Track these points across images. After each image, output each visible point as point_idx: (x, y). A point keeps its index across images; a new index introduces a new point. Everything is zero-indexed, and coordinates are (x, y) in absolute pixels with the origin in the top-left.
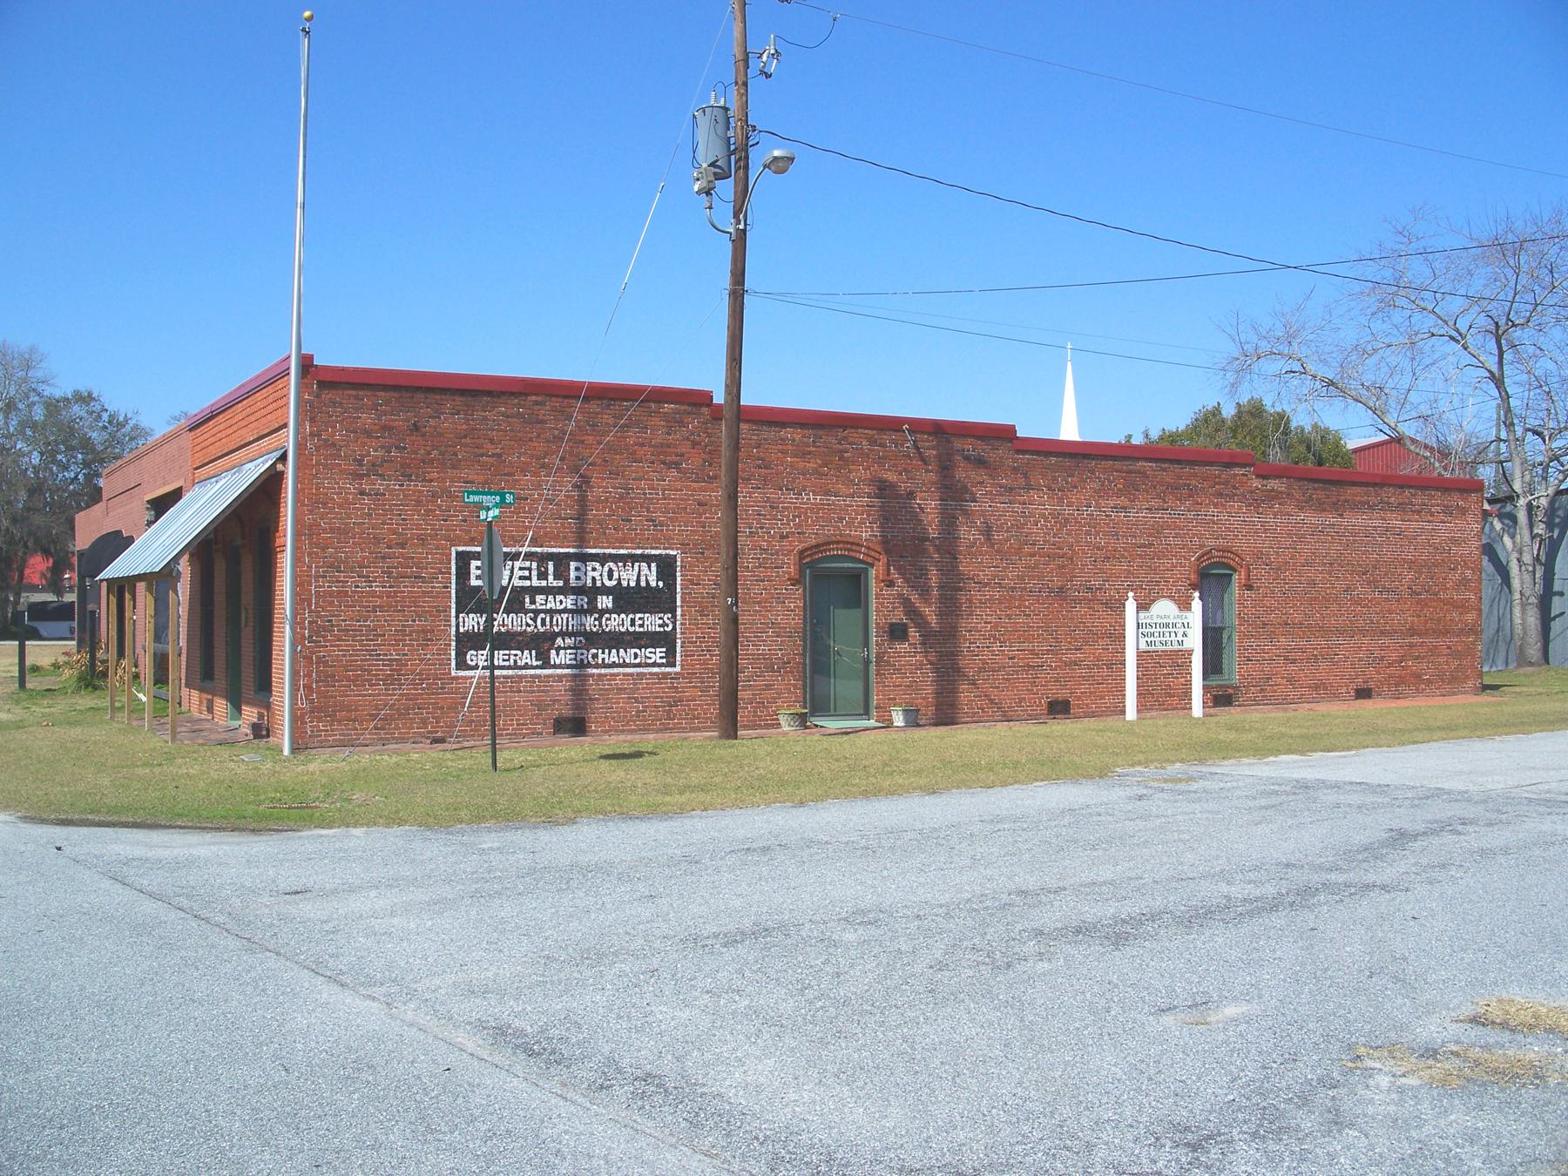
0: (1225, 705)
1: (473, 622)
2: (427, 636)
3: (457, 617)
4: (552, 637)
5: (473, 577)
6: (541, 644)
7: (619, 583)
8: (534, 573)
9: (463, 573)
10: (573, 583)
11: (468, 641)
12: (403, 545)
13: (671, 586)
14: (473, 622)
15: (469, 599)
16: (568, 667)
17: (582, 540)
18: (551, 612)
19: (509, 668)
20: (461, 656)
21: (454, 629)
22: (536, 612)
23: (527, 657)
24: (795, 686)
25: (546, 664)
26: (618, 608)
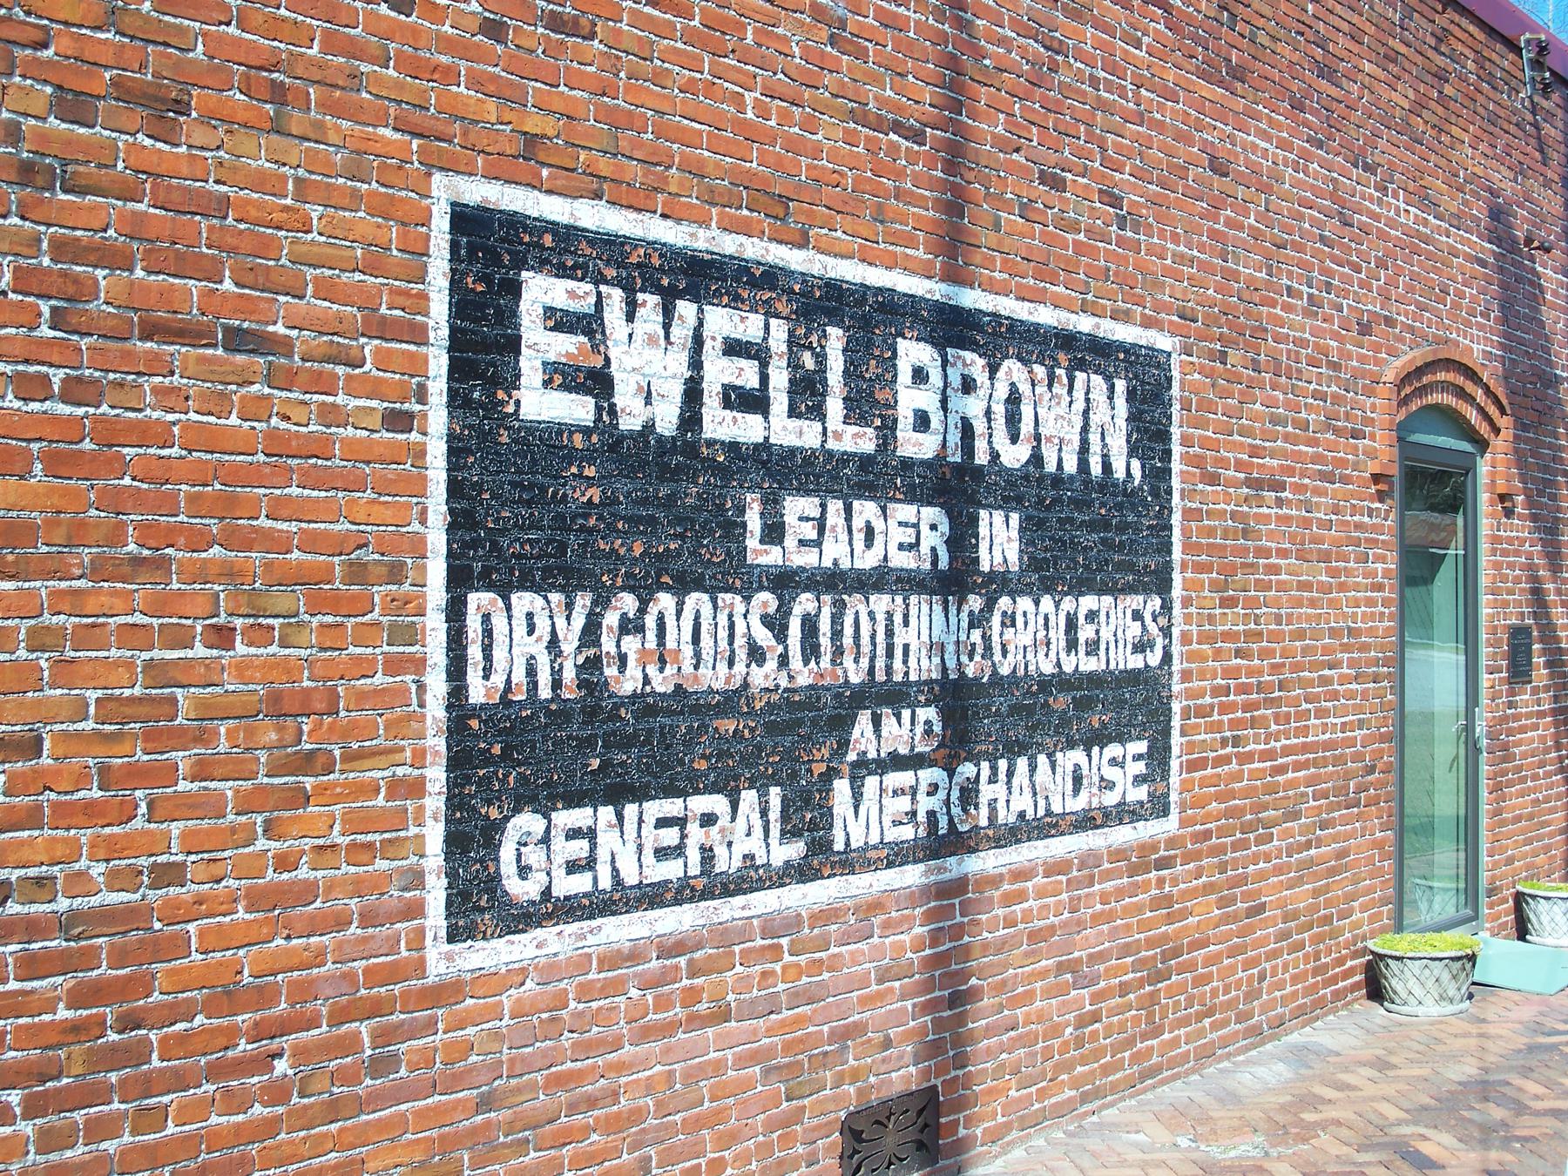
0: (738, 341)
1: (526, 641)
2: (304, 735)
3: (455, 612)
4: (831, 713)
5: (530, 367)
6: (788, 748)
7: (1037, 459)
8: (779, 378)
9: (484, 349)
10: (917, 446)
11: (518, 756)
12: (164, 109)
13: (1159, 476)
14: (526, 641)
15: (538, 510)
16: (898, 856)
17: (954, 253)
18: (834, 582)
19: (683, 893)
20: (471, 840)
21: (437, 684)
22: (785, 582)
23: (745, 828)
24: (1379, 844)
25: (821, 858)
26: (1047, 570)
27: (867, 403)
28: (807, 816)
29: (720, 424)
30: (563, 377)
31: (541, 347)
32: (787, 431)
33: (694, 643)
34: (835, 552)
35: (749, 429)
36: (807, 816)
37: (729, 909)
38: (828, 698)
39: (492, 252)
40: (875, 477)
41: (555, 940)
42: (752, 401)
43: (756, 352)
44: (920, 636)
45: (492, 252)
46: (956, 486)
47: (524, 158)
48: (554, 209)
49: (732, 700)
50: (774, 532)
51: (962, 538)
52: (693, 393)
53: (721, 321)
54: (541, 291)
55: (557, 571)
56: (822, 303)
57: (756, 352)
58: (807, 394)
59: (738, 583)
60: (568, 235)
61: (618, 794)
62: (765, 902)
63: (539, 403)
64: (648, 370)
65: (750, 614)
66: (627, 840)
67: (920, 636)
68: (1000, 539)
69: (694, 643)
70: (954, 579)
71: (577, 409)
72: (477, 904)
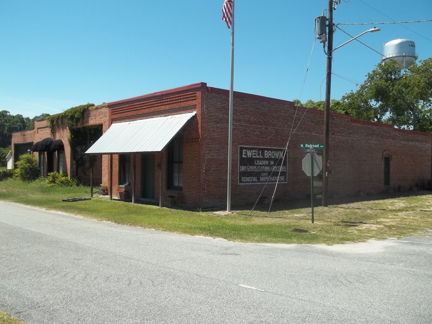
1: (243, 168)
9: (241, 154)
14: (243, 168)
19: (251, 182)
20: (240, 178)
22: (257, 165)
23: (255, 179)
27: (263, 155)
28: (258, 179)
29: (253, 157)
30: (245, 155)
31: (244, 153)
32: (257, 157)
33: (252, 168)
34: (260, 164)
35: (255, 157)
36: (258, 179)
37: (254, 184)
38: (4, 160)
39: (242, 149)
40: (264, 159)
41: (244, 184)
42: (255, 155)
43: (256, 153)
44: (267, 169)
45: (242, 149)
46: (270, 159)
47: (243, 144)
48: (244, 146)
49: (254, 172)
50: (257, 163)
51: (269, 163)
52: (252, 155)
53: (253, 151)
54: (244, 151)
55: (245, 165)
56: (259, 149)
57: (256, 153)
58: (259, 155)
59: (426, 117)
60: (245, 147)
61: (247, 176)
62: (256, 183)
63: (244, 156)
64: (249, 154)
65: (255, 167)
66: (248, 179)
67: (267, 169)
68: (272, 163)
69: (252, 168)
70: (269, 165)
71: (245, 157)
72: (241, 181)
